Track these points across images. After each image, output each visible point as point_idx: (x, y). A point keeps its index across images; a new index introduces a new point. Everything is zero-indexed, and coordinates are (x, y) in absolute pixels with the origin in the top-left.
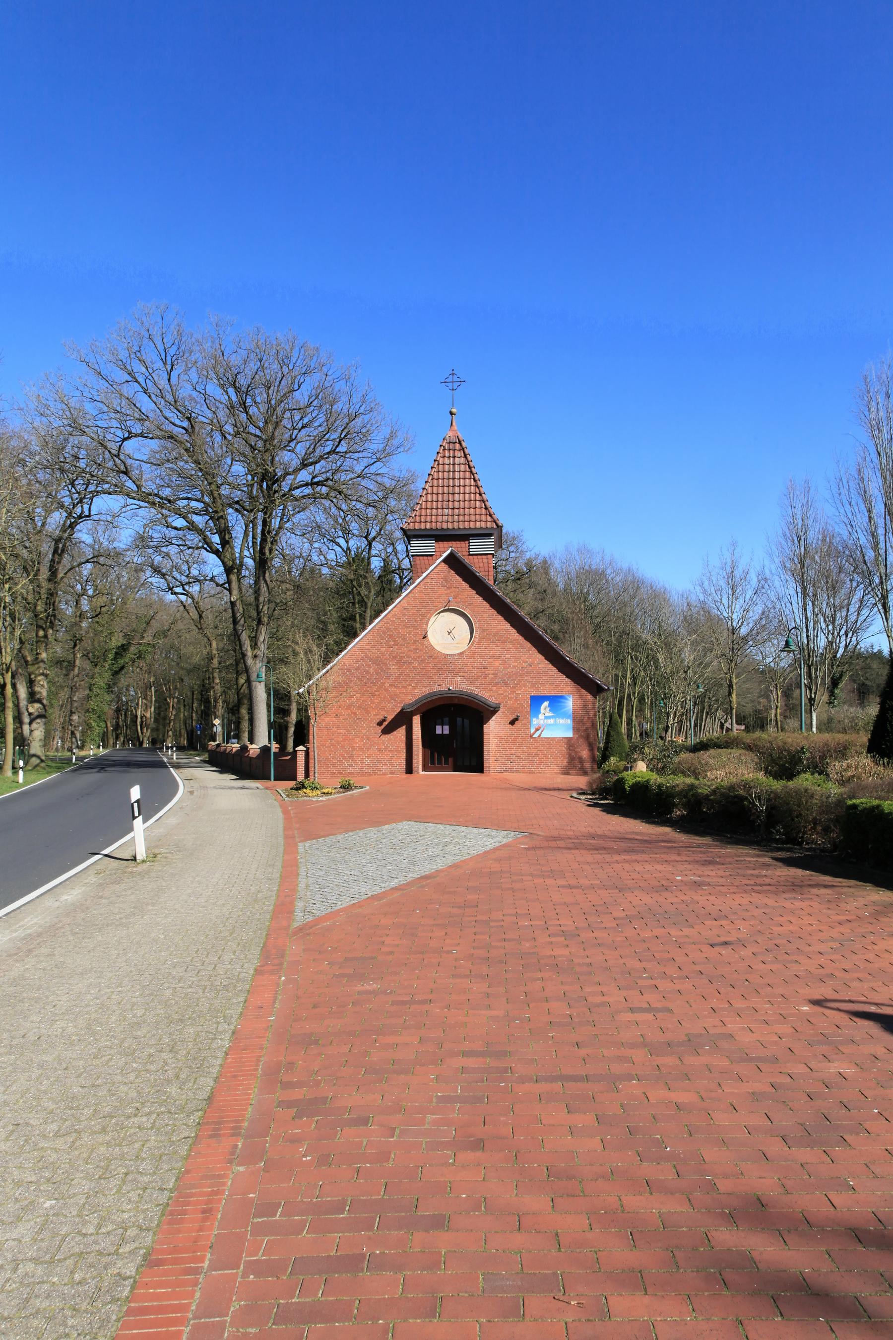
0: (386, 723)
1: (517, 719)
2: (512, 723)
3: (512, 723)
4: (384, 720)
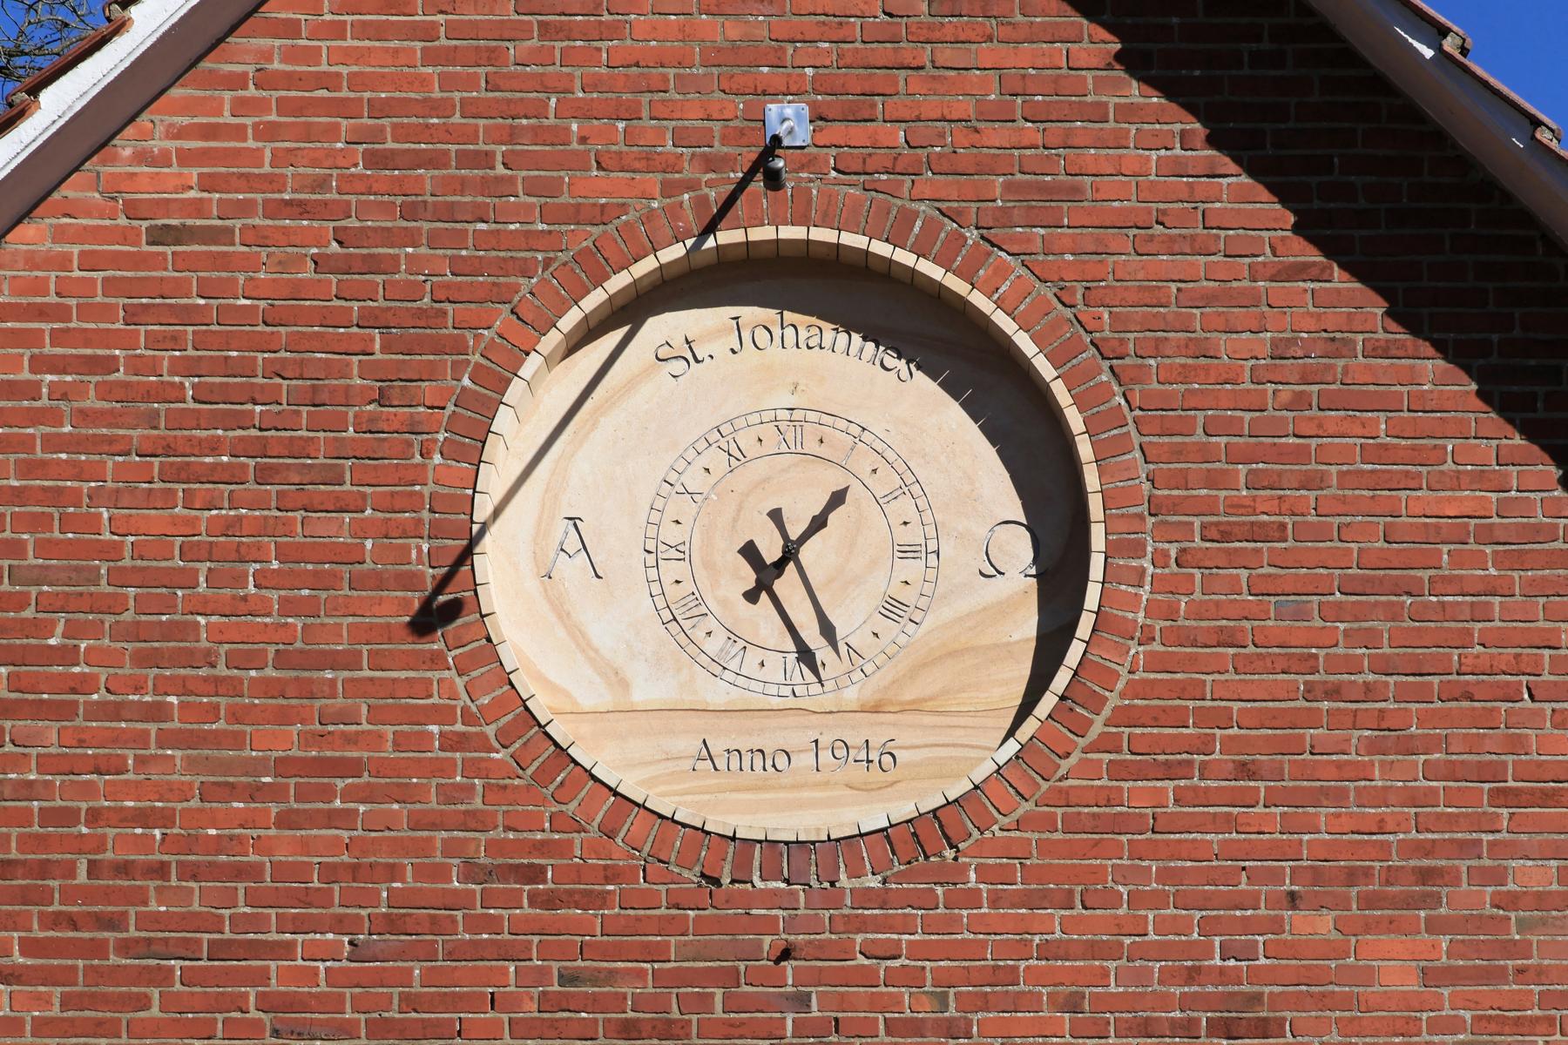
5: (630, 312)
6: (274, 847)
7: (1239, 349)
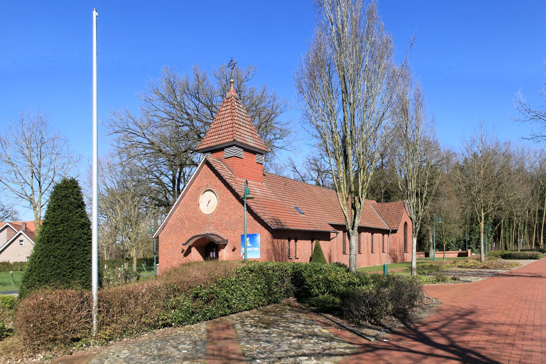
0: (184, 252)
1: (235, 248)
2: (233, 250)
3: (233, 250)
4: (184, 250)
5: (205, 192)
6: (193, 216)
7: (222, 191)
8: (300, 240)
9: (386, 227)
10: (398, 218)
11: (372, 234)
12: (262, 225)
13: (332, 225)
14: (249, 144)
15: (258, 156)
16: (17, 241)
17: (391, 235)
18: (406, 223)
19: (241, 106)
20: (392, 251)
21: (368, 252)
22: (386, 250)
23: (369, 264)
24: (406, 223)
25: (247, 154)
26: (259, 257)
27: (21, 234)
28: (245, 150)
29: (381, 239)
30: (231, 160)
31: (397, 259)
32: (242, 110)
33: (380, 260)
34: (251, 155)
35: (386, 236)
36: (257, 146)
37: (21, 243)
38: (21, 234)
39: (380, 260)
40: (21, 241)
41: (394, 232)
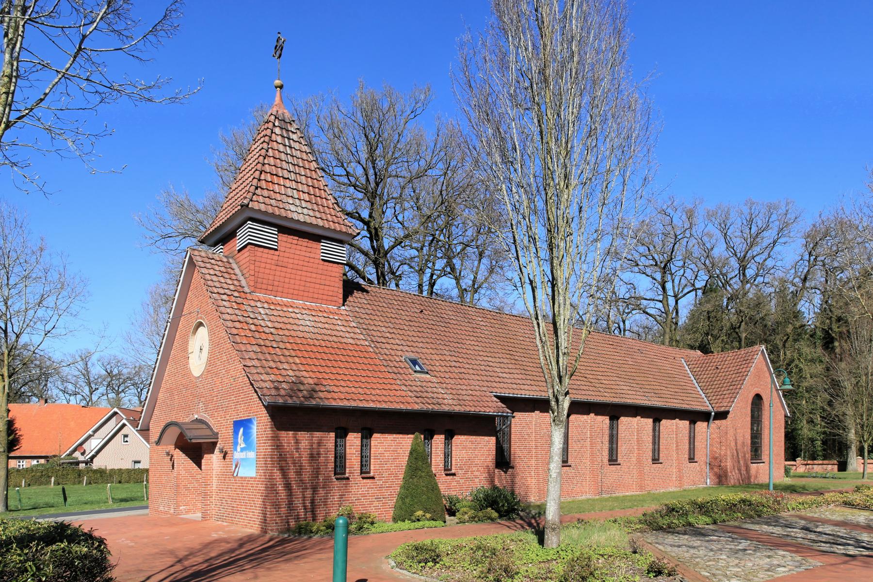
8: (382, 432)
9: (706, 405)
10: (735, 387)
11: (614, 418)
12: (635, 416)
13: (503, 399)
14: (295, 216)
15: (324, 245)
16: (120, 436)
17: (715, 424)
18: (758, 398)
19: (295, 137)
20: (716, 459)
21: (639, 461)
22: (700, 455)
23: (641, 488)
24: (758, 398)
25: (284, 237)
26: (254, 476)
27: (124, 425)
28: (283, 230)
29: (686, 432)
30: (330, 269)
31: (726, 476)
32: (297, 146)
33: (680, 478)
34: (304, 242)
35: (701, 426)
36: (314, 221)
37: (126, 439)
38: (124, 425)
39: (680, 478)
40: (126, 436)
41: (722, 415)
